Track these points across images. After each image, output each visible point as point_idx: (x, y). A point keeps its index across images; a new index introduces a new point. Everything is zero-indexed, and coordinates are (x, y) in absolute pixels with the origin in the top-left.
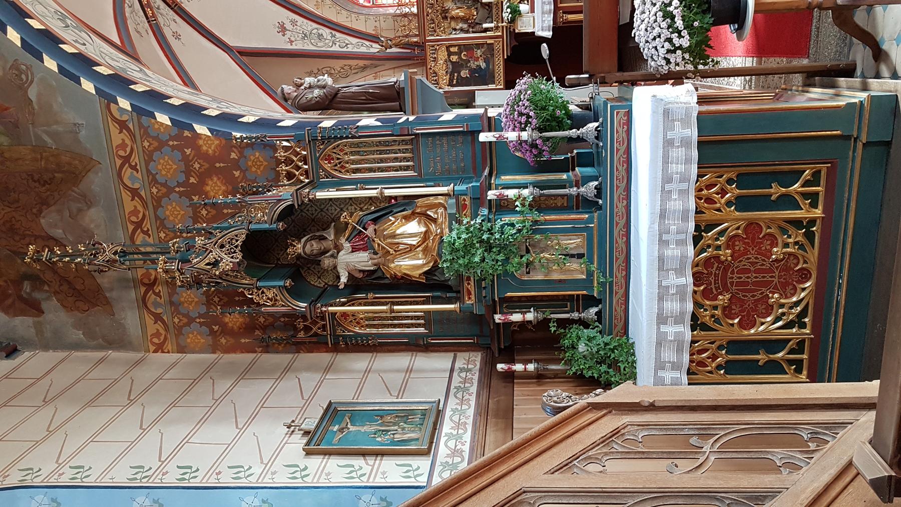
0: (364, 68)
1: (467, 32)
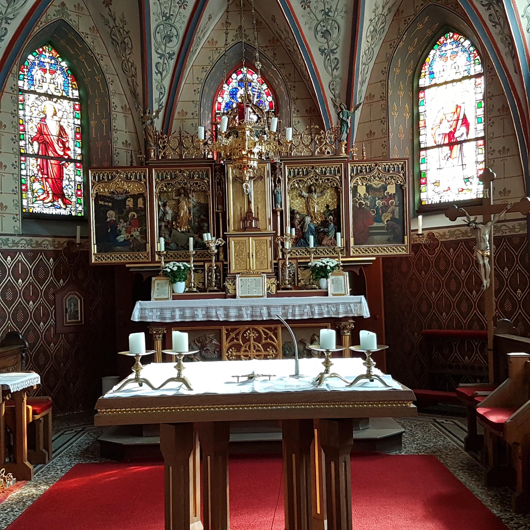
0: (134, 94)
1: (161, 220)
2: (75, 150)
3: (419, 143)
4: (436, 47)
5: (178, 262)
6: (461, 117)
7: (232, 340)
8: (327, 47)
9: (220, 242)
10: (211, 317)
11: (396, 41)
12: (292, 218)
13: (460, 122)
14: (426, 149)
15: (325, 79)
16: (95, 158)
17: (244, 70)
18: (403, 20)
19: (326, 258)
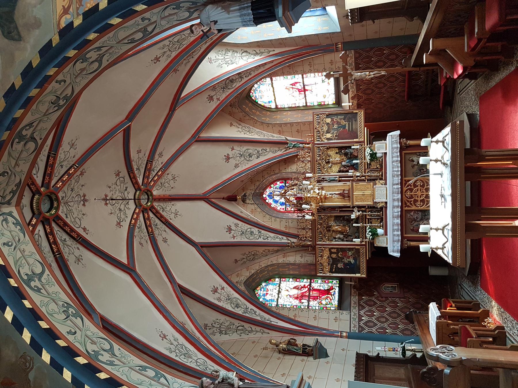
0: (277, 251)
1: (343, 240)
2: (305, 282)
3: (304, 106)
4: (257, 101)
5: (366, 232)
6: (291, 86)
7: (411, 204)
9: (356, 210)
10: (398, 215)
12: (343, 172)
13: (294, 87)
14: (306, 103)
15: (271, 155)
16: (310, 272)
19: (365, 154)
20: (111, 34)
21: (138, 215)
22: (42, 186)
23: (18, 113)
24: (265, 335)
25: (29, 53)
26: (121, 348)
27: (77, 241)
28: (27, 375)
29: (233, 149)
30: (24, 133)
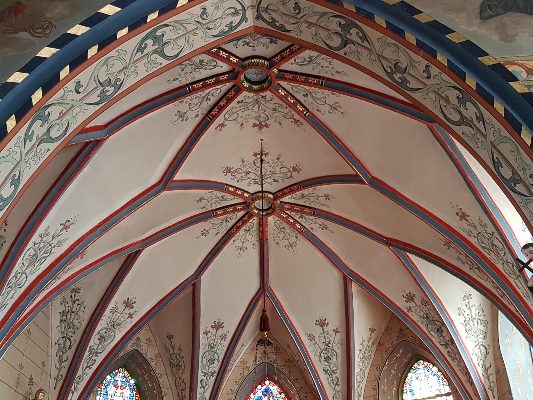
4: (412, 371)
8: (329, 369)
11: (381, 365)
17: (267, 382)
18: (384, 350)
20: (505, 133)
21: (241, 196)
22: (279, 70)
23: (380, 21)
24: (53, 382)
25: (465, 28)
26: (50, 153)
27: (207, 115)
28: (26, 31)
29: (336, 332)
30: (354, 31)
